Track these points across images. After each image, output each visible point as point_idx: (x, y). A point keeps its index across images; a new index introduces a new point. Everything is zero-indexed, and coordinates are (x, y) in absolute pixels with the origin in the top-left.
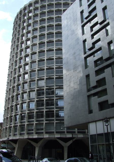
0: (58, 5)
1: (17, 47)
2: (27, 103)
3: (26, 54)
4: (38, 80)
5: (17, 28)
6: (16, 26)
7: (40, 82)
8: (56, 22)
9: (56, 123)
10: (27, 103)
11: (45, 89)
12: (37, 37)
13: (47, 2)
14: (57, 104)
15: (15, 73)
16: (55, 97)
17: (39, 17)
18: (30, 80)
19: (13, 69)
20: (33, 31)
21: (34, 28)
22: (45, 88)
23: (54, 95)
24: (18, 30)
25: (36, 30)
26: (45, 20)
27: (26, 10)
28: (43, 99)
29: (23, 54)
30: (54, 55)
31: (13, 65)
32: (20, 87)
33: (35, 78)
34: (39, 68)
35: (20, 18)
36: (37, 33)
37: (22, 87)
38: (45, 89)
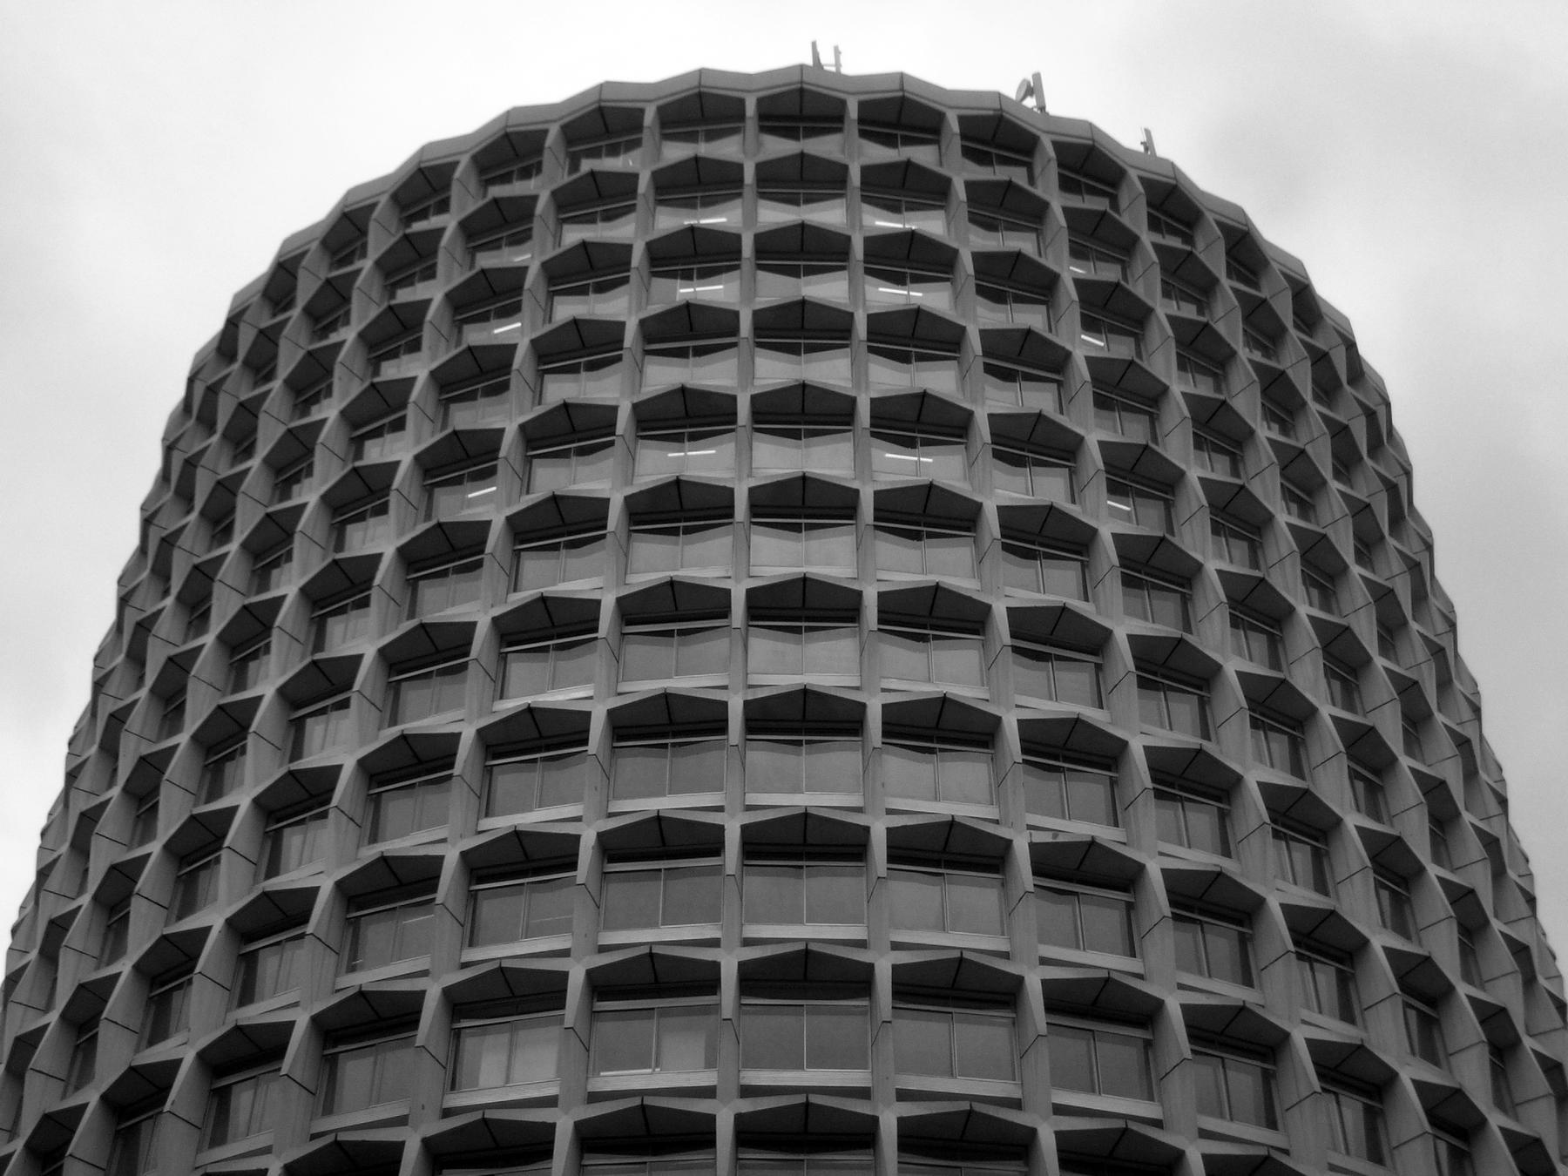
24: (103, 856)
27: (276, 564)
29: (203, 1018)
35: (90, 999)
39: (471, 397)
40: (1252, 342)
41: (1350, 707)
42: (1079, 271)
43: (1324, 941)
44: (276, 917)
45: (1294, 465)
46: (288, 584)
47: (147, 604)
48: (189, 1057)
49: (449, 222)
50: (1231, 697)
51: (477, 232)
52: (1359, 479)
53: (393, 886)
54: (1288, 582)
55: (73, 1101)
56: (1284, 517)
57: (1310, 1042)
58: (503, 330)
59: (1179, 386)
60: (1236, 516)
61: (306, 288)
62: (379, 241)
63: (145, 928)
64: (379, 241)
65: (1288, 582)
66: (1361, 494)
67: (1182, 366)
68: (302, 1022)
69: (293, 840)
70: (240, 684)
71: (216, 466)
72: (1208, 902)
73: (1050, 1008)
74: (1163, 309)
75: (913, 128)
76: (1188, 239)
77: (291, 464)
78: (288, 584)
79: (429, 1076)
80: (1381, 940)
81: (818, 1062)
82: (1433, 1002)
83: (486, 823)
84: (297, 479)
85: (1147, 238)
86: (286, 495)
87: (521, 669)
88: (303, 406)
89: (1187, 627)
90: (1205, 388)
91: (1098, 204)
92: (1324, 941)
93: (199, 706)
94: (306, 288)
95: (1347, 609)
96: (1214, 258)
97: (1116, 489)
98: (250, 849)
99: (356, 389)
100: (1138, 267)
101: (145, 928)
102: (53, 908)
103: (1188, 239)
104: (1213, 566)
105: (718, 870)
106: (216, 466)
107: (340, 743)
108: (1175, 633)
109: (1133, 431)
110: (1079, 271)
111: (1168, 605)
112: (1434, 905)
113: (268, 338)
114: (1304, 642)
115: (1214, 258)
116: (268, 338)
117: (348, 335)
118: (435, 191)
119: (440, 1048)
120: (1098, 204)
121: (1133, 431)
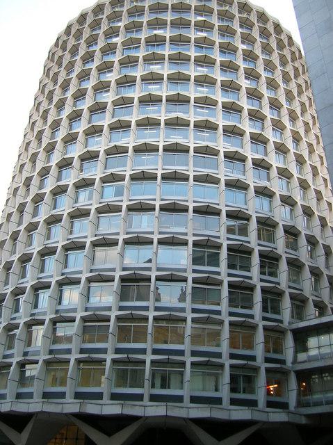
0: (181, 8)
1: (33, 163)
2: (40, 363)
3: (60, 183)
4: (89, 280)
5: (31, 145)
6: (41, 98)
7: (100, 252)
8: (156, 341)
9: (153, 362)
10: (40, 363)
11: (113, 319)
12: (98, 156)
13: (147, 1)
14: (158, 299)
15: (21, 217)
16: (152, 308)
17: (108, 114)
18: (55, 316)
19: (10, 234)
20: (82, 160)
21: (85, 150)
22: (113, 314)
23: (151, 303)
25: (92, 158)
26: (130, 126)
28: (107, 313)
30: (157, 164)
31: (12, 219)
32: (23, 298)
33: (86, 237)
34: (96, 270)
36: (104, 119)
37: (56, 177)
38: (113, 319)
39: (108, 54)
40: (281, 65)
41: (296, 150)
42: (245, 47)
43: (284, 174)
44: (60, 191)
45: (289, 94)
46: (69, 94)
47: (35, 117)
48: (42, 221)
49: (101, 32)
50: (271, 147)
51: (110, 19)
52: (299, 78)
53: (90, 157)
54: (283, 100)
55: (19, 229)
56: (285, 105)
57: (283, 225)
58: (115, 40)
59: (264, 75)
60: (272, 85)
61: (73, 31)
62: (89, 20)
63: (34, 190)
64: (89, 20)
65: (283, 100)
66: (299, 82)
67: (262, 53)
68: (71, 184)
69: (64, 172)
70: (48, 161)
71: (50, 87)
72: (260, 165)
73: (225, 157)
74: (261, 57)
75: (209, 63)
76: (268, 40)
77: (65, 87)
78: (69, 94)
79: (96, 196)
80: (296, 175)
81: (177, 195)
82: (305, 189)
83: (106, 171)
84: (66, 90)
85: (259, 40)
86: (64, 95)
87: (115, 136)
88: (68, 74)
89: (266, 155)
90: (267, 58)
91: (248, 32)
92: (284, 174)
93: (45, 141)
94: (73, 31)
95: (295, 106)
96: (271, 28)
97: (246, 78)
98: (50, 203)
99: (80, 70)
100: (252, 14)
101: (34, 190)
102: (15, 186)
103: (268, 40)
104: (269, 116)
105: (158, 155)
106: (50, 87)
107: (75, 152)
108: (259, 132)
109: (250, 66)
110: (245, 47)
111: (256, 103)
112: (308, 169)
113: (65, 42)
114: (288, 134)
115: (271, 28)
116: (65, 42)
117: (78, 58)
118: (95, 40)
119: (99, 190)
120: (248, 32)
121: (250, 66)
